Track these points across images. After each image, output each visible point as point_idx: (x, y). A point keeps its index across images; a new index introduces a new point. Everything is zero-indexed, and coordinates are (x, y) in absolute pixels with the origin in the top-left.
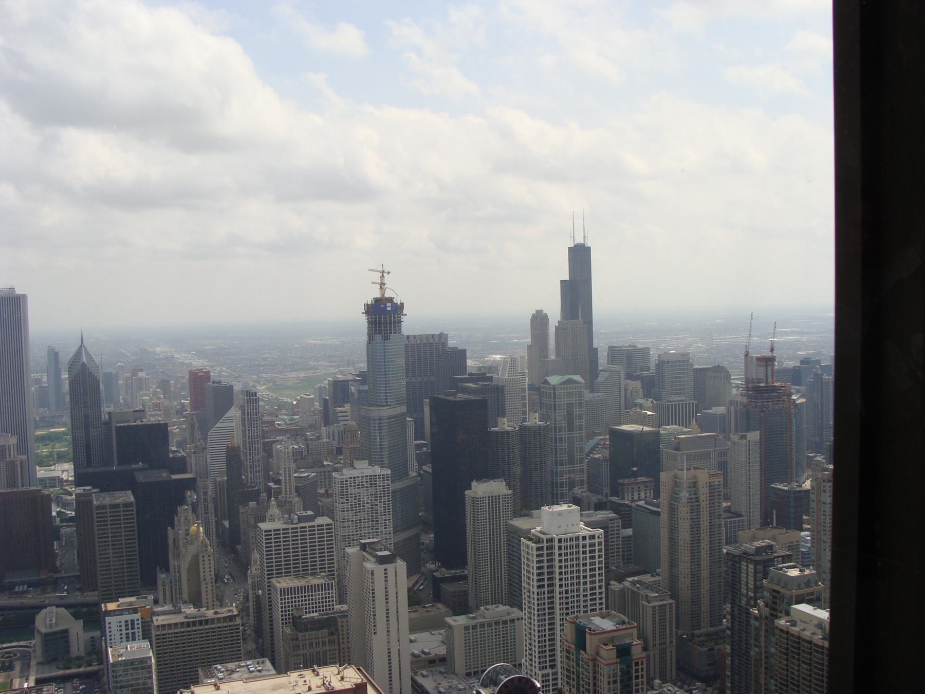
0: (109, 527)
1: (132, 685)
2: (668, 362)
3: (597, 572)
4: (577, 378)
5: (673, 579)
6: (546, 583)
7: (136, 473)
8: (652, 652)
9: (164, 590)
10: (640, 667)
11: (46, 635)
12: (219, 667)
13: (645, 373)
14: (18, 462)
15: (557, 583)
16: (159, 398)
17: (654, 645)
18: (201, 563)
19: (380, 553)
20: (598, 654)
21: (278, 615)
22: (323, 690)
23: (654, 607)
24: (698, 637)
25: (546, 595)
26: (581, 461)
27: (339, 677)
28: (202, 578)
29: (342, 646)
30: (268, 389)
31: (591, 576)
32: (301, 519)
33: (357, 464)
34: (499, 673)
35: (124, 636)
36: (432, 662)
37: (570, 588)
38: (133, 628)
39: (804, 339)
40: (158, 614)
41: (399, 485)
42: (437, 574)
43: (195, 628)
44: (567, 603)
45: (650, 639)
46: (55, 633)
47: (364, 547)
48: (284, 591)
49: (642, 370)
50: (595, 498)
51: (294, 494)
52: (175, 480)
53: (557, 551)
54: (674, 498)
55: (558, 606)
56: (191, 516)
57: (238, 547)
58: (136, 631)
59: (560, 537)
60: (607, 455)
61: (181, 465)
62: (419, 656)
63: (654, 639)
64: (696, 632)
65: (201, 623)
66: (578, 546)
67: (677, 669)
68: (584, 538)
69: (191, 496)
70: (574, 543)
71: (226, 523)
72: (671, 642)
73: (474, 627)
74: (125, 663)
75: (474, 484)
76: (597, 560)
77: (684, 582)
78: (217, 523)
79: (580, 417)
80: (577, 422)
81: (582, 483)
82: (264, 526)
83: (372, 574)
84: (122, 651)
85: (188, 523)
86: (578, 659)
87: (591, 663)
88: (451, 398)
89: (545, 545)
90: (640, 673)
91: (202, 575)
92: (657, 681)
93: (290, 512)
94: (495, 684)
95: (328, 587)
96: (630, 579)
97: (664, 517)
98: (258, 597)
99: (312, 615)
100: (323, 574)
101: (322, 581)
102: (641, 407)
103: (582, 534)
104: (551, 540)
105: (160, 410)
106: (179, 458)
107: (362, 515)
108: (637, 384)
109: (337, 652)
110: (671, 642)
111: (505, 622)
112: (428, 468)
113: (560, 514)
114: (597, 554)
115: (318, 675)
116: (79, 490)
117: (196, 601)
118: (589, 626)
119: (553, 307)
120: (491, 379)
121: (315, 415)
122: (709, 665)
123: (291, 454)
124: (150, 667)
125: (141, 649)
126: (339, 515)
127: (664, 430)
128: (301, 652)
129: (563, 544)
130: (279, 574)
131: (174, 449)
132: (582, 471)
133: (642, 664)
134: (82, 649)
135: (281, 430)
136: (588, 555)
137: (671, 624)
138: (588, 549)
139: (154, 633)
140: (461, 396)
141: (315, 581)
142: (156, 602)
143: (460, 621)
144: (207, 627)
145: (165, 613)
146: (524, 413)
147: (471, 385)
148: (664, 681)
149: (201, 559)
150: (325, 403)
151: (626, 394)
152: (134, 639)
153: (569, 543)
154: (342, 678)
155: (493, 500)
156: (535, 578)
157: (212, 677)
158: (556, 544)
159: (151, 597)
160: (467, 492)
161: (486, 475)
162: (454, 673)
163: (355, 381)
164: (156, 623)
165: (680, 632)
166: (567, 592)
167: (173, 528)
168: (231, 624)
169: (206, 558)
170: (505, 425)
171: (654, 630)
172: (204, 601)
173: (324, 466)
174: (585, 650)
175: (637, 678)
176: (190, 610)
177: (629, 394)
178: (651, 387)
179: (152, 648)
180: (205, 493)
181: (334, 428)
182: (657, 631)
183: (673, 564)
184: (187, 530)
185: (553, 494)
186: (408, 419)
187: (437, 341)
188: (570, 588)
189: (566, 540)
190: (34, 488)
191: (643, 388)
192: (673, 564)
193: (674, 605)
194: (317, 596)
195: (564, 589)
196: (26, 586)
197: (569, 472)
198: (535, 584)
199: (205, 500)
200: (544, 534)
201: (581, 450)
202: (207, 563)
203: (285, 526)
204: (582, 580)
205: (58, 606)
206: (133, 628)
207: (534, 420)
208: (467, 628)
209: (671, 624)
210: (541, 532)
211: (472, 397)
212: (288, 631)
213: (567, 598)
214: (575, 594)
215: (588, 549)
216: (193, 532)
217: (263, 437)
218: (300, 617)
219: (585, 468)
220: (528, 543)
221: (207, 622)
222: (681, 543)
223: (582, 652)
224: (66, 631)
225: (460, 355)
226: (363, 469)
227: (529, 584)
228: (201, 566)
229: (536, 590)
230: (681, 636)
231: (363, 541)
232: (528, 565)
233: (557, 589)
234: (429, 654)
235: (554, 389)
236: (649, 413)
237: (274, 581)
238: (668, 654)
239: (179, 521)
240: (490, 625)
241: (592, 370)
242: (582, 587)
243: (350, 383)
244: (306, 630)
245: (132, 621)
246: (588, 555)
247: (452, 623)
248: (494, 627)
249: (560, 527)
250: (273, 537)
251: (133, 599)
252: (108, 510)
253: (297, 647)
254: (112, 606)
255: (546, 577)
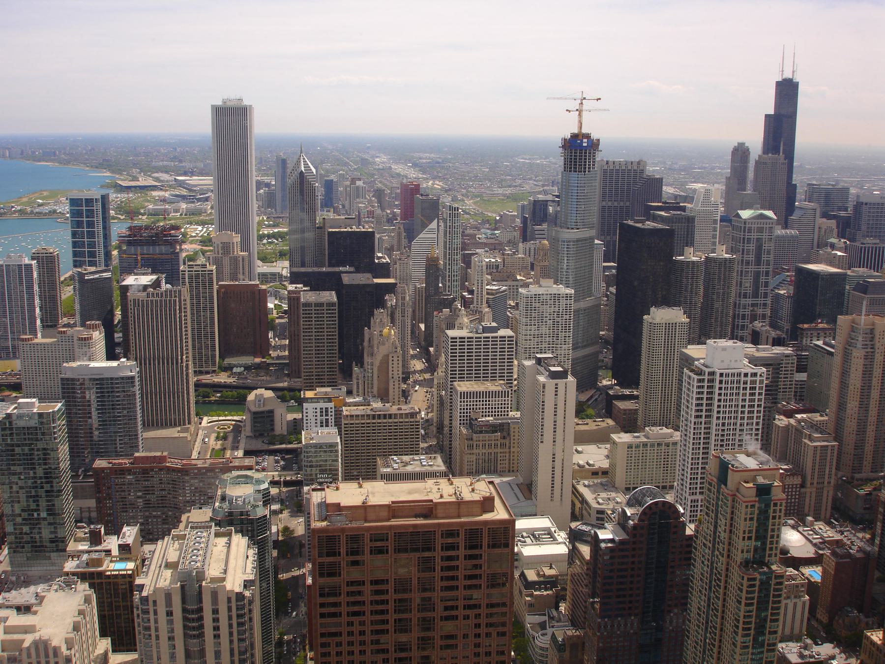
0: (313, 323)
1: (320, 466)
2: (866, 204)
3: (756, 409)
4: (770, 213)
5: (839, 422)
6: (704, 414)
7: (343, 275)
8: (808, 490)
9: (358, 384)
10: (778, 508)
11: (255, 413)
12: (395, 458)
13: (842, 214)
14: (241, 259)
15: (715, 415)
16: (373, 207)
17: (812, 484)
18: (390, 363)
19: (552, 369)
20: (738, 490)
21: (457, 415)
22: (453, 499)
23: (816, 447)
24: (858, 480)
25: (703, 426)
26: (766, 295)
27: (470, 488)
28: (390, 376)
29: (512, 450)
30: (475, 203)
31: (749, 412)
32: (485, 330)
33: (543, 282)
34: (644, 495)
35: (319, 422)
36: (595, 473)
37: (726, 421)
38: (327, 415)
39: (366, 344)
40: (346, 404)
41: (582, 305)
42: (611, 392)
43: (379, 421)
44: (723, 435)
45: (809, 477)
46: (263, 412)
47: (539, 361)
48: (464, 395)
49: (840, 209)
50: (773, 334)
51: (485, 305)
52: (377, 284)
53: (717, 385)
54: (849, 344)
55: (713, 437)
56: (387, 320)
57: (431, 349)
58: (329, 417)
59: (722, 371)
60: (792, 292)
61: (383, 270)
62: (583, 466)
63: (812, 478)
64: (857, 476)
65: (385, 416)
66: (739, 382)
67: (832, 508)
68: (746, 375)
69: (391, 300)
70: (736, 378)
71: (422, 326)
72: (829, 483)
73: (637, 446)
74: (315, 446)
75: (653, 309)
76: (757, 397)
77: (851, 425)
78: (413, 326)
79: (769, 253)
80: (764, 257)
81: (764, 316)
82: (451, 333)
83: (544, 387)
84: (313, 435)
85: (383, 325)
86: (718, 492)
87: (730, 498)
88: (639, 225)
89: (706, 377)
90: (778, 514)
91: (390, 373)
92: (810, 518)
93: (480, 320)
94: (640, 505)
95: (504, 394)
96: (799, 416)
97: (837, 360)
98: (441, 396)
99: (488, 418)
100: (502, 382)
101: (500, 388)
102: (833, 246)
103: (744, 371)
104: (712, 374)
105: (373, 217)
106: (384, 263)
107: (544, 330)
108: (833, 223)
109: (507, 455)
110: (829, 483)
111: (667, 445)
112: (613, 290)
113: (724, 349)
114: (757, 391)
115: (452, 484)
116: (291, 287)
117: (384, 396)
118: (733, 462)
119: (754, 138)
120: (683, 209)
121: (515, 231)
122: (865, 509)
123: (484, 268)
124: (337, 451)
125: (330, 435)
126: (522, 329)
127: (853, 272)
128: (475, 451)
129: (724, 379)
130: (462, 379)
131: (380, 255)
132: (765, 305)
133: (781, 505)
134: (285, 428)
135: (482, 243)
136: (748, 391)
137: (831, 465)
138: (748, 386)
139: (344, 422)
140: (650, 225)
141: (490, 386)
142: (349, 393)
143: (624, 438)
144: (390, 421)
145: (356, 404)
146: (714, 244)
147: (663, 213)
148: (817, 519)
149: (391, 359)
150: (524, 220)
151: (819, 232)
152: (327, 426)
153: (730, 378)
154: (473, 490)
155: (670, 327)
156: (694, 408)
157: (388, 466)
158: (718, 378)
159: (344, 389)
160: (645, 317)
161: (667, 302)
162: (614, 487)
163: (554, 201)
164: (345, 413)
165: (840, 474)
166: (723, 425)
167: (369, 328)
168: (412, 420)
169: (395, 359)
170: (692, 255)
171: (813, 469)
172: (391, 397)
173: (518, 280)
174: (726, 485)
175: (774, 518)
176: (377, 405)
177: (823, 233)
178: (846, 228)
179: (340, 434)
180: (403, 298)
181: (531, 244)
182: (817, 470)
183: (841, 406)
184: (381, 331)
185: (733, 325)
186: (597, 242)
187: (635, 168)
188: (726, 421)
189: (727, 375)
190: (253, 283)
191: (838, 227)
192: (841, 406)
193: (836, 447)
194: (494, 402)
195: (721, 421)
196: (242, 369)
197: (753, 305)
198: (694, 414)
199: (403, 304)
200: (707, 367)
201: (766, 284)
202: (395, 362)
203: (471, 335)
204: (740, 415)
205: (266, 389)
206: (327, 415)
207: (722, 253)
208: (630, 446)
209: (831, 465)
210: (703, 365)
211: (660, 226)
212: (464, 431)
213: (723, 430)
214: (732, 427)
215: (748, 386)
216: (385, 333)
217: (463, 249)
218: (476, 419)
219: (769, 302)
220: (690, 374)
221: (390, 416)
222: (851, 387)
223: (723, 486)
224: (272, 412)
225: (656, 184)
226: (550, 287)
227: (687, 413)
228: (390, 366)
229: (693, 420)
230: (841, 478)
231: (538, 356)
232: (688, 395)
233: (715, 421)
234: (593, 465)
235: (745, 223)
236: (839, 253)
237: (455, 383)
238: (825, 493)
239: (375, 323)
240: (652, 445)
241: (787, 208)
242: (739, 422)
243: (549, 203)
244: (481, 432)
245: (326, 408)
246: (748, 391)
247: (617, 440)
248: (656, 448)
249: (722, 361)
250: (458, 344)
251: (329, 389)
252: (313, 308)
253: (471, 447)
254: (309, 394)
255: (704, 408)
